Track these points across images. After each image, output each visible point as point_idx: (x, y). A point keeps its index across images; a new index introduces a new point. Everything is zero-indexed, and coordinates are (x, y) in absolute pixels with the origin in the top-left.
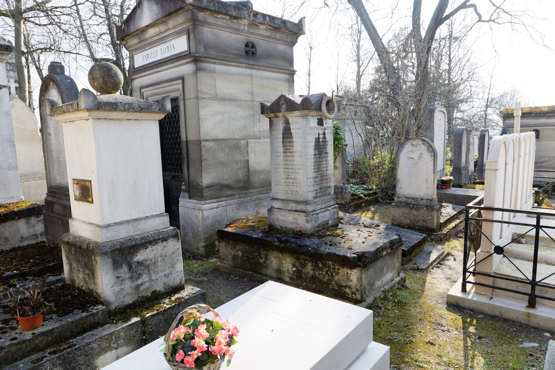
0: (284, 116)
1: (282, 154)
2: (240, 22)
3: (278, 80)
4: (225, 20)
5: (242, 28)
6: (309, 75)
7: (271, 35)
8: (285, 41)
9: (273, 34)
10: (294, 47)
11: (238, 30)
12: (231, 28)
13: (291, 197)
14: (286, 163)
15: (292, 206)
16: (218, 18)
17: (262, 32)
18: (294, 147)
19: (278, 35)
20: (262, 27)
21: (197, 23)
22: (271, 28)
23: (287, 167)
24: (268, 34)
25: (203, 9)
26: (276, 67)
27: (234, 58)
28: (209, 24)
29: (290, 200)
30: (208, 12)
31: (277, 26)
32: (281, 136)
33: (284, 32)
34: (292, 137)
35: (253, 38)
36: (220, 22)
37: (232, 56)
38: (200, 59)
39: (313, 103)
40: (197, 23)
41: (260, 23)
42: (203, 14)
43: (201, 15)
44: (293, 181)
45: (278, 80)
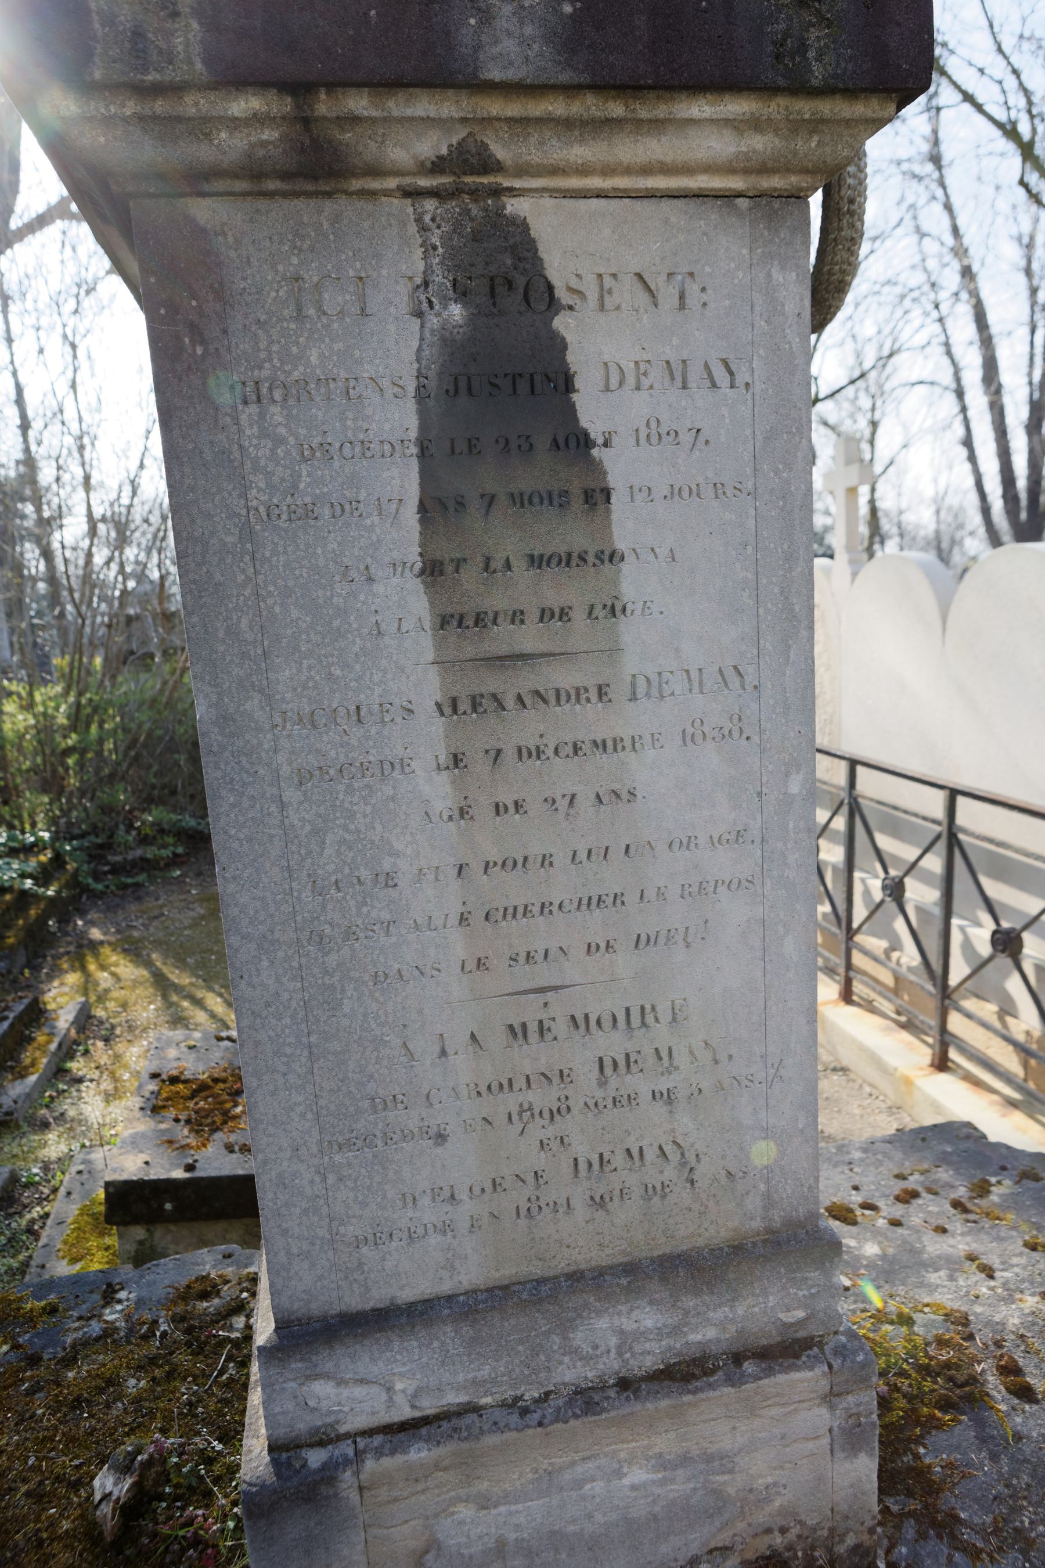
0: (467, 169)
1: (428, 737)
6: (10, 340)
13: (579, 1239)
14: (488, 840)
15: (638, 1329)
18: (631, 632)
23: (515, 890)
29: (576, 1278)
32: (404, 481)
34: (597, 497)
44: (612, 1044)
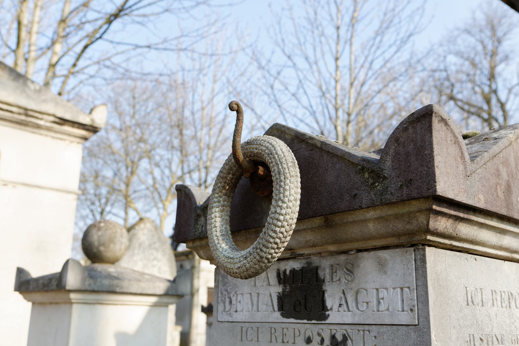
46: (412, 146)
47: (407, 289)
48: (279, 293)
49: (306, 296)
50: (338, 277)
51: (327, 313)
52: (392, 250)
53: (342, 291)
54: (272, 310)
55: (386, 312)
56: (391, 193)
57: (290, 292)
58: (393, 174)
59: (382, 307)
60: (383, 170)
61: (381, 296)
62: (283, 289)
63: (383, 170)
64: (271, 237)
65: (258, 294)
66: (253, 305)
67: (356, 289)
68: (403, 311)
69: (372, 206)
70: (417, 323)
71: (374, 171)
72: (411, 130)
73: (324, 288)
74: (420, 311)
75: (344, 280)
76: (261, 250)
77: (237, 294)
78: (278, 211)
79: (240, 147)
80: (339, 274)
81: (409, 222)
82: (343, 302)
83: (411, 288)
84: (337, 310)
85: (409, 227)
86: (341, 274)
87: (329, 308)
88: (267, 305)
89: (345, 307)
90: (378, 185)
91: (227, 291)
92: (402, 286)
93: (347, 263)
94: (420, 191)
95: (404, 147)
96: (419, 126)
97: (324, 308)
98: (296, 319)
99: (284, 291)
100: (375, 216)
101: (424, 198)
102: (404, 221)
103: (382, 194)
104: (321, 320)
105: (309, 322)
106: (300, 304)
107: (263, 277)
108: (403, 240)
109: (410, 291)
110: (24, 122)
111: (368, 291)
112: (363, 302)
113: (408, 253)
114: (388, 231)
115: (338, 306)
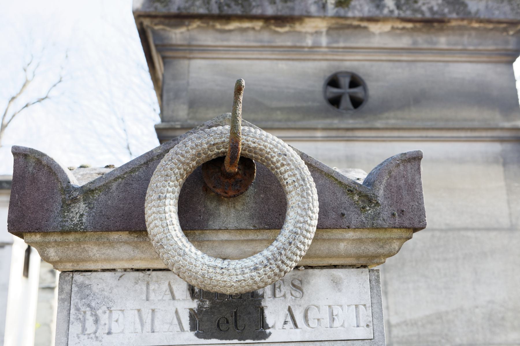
2: (298, 27)
3: (461, 161)
4: (251, 33)
5: (309, 42)
7: (415, 43)
8: (477, 52)
9: (422, 40)
10: (515, 64)
11: (296, 49)
12: (274, 48)
16: (230, 31)
17: (376, 42)
19: (443, 41)
20: (374, 28)
21: (169, 54)
22: (409, 25)
24: (405, 42)
25: (181, 18)
26: (450, 125)
27: (288, 120)
28: (204, 49)
30: (196, 24)
31: (428, 15)
33: (461, 28)
35: (352, 63)
36: (236, 40)
37: (279, 115)
38: (171, 133)
39: (76, 180)
40: (169, 54)
41: (362, 19)
42: (183, 29)
43: (177, 35)
45: (461, 161)
46: (403, 181)
47: (363, 307)
48: (191, 309)
49: (236, 313)
50: (282, 293)
51: (268, 331)
52: (347, 269)
53: (288, 307)
54: (179, 330)
55: (342, 328)
56: (384, 220)
57: (211, 308)
58: (386, 202)
59: (337, 323)
60: (377, 197)
61: (335, 313)
62: (199, 305)
63: (377, 197)
64: (298, 248)
65: (153, 311)
66: (142, 324)
67: (306, 306)
68: (358, 326)
69: (362, 227)
70: (372, 338)
71: (368, 196)
72: (402, 168)
73: (263, 304)
74: (375, 327)
75: (290, 296)
76: (283, 262)
77: (111, 311)
78: (309, 222)
79: (164, 124)
80: (286, 289)
81: (382, 247)
82: (289, 319)
83: (367, 305)
84: (281, 328)
85: (381, 251)
86: (287, 289)
87: (270, 326)
88: (171, 324)
89: (291, 324)
90: (369, 210)
91: (89, 305)
92: (357, 304)
93: (294, 279)
94: (412, 223)
95: (396, 180)
96: (409, 166)
97: (265, 326)
98: (221, 339)
99: (200, 307)
100: (355, 237)
101: (406, 228)
102: (378, 245)
103: (373, 219)
104: (244, 340)
105: (242, 342)
106: (228, 322)
107: (164, 289)
108: (353, 261)
109: (366, 308)
110: (173, 21)
111: (321, 307)
112: (314, 319)
113: (364, 273)
114: (358, 252)
115: (283, 323)
